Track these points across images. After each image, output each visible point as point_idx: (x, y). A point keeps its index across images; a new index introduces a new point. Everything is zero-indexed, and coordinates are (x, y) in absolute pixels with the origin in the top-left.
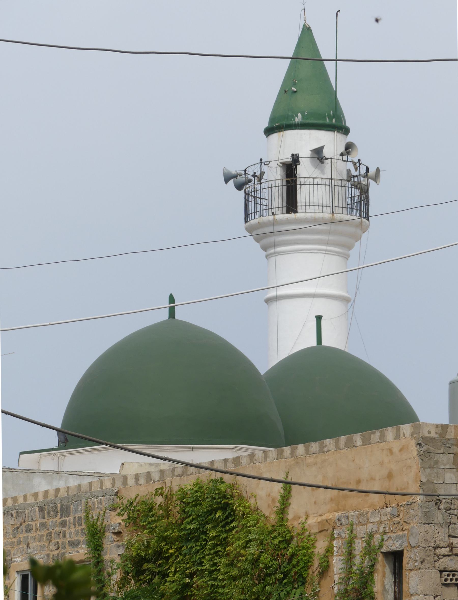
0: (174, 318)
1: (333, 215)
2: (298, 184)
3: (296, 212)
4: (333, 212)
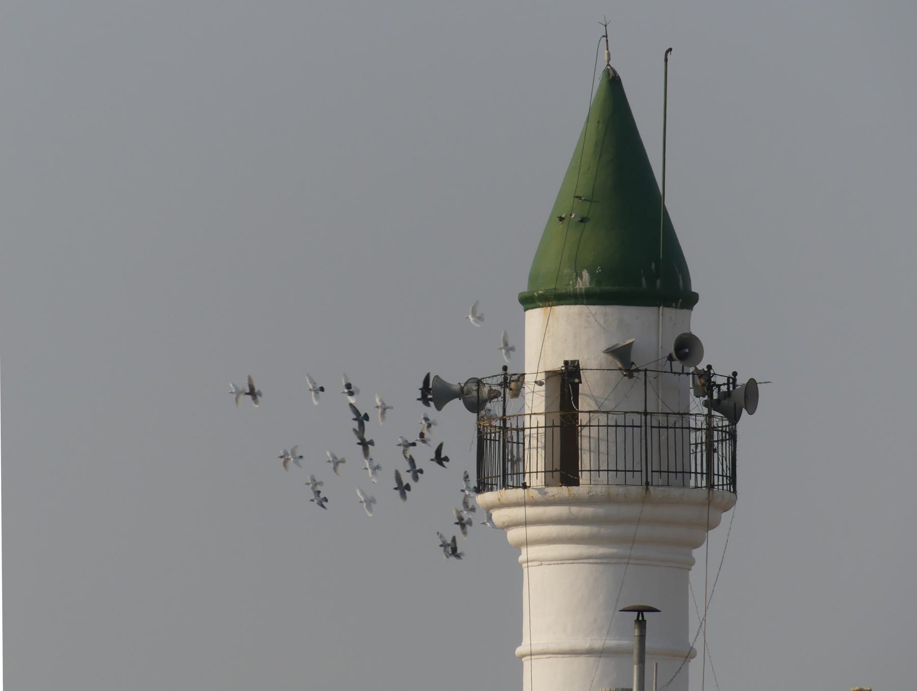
0: (526, 310)
1: (647, 489)
2: (558, 473)
3: (577, 483)
4: (647, 483)
